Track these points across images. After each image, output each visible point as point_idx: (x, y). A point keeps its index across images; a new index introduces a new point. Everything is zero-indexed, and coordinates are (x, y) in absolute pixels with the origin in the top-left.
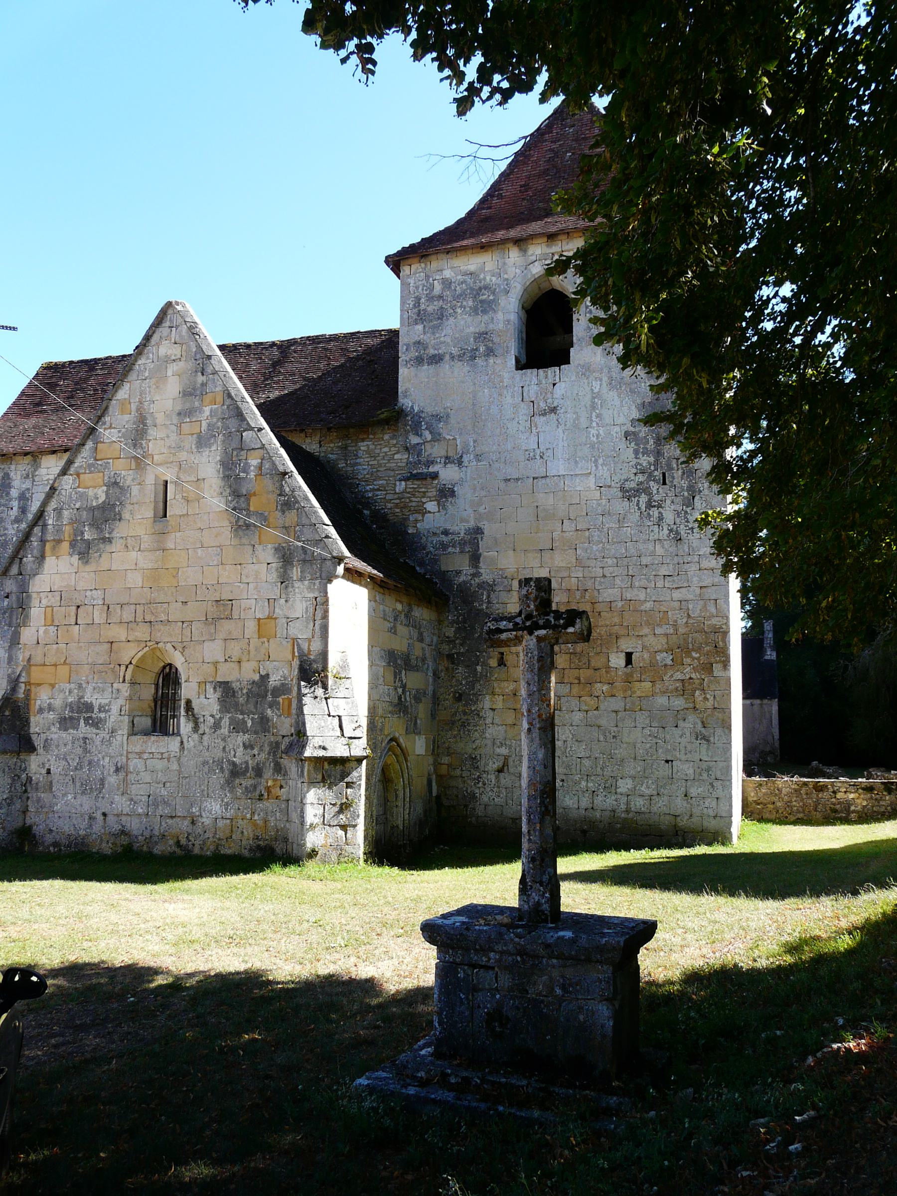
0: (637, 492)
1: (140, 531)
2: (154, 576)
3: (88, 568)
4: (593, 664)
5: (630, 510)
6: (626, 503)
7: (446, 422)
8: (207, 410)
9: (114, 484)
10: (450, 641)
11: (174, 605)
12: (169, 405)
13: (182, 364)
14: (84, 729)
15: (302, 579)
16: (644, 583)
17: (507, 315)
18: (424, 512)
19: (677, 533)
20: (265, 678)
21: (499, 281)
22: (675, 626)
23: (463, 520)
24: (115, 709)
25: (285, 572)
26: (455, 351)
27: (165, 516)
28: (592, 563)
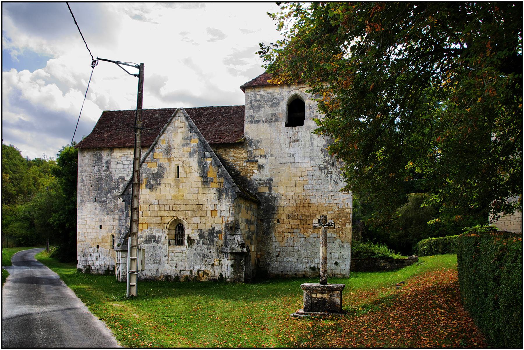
0: (324, 169)
1: (171, 182)
2: (176, 196)
3: (152, 193)
4: (308, 223)
5: (322, 174)
6: (320, 172)
7: (261, 143)
8: (192, 145)
9: (160, 166)
10: (261, 215)
11: (182, 206)
12: (179, 142)
13: (183, 129)
14: (153, 244)
15: (225, 199)
16: (325, 198)
17: (283, 107)
18: (253, 173)
19: (337, 182)
20: (213, 229)
21: (280, 96)
22: (334, 211)
23: (266, 176)
24: (163, 238)
25: (220, 196)
26: (264, 119)
27: (178, 177)
28: (308, 191)
